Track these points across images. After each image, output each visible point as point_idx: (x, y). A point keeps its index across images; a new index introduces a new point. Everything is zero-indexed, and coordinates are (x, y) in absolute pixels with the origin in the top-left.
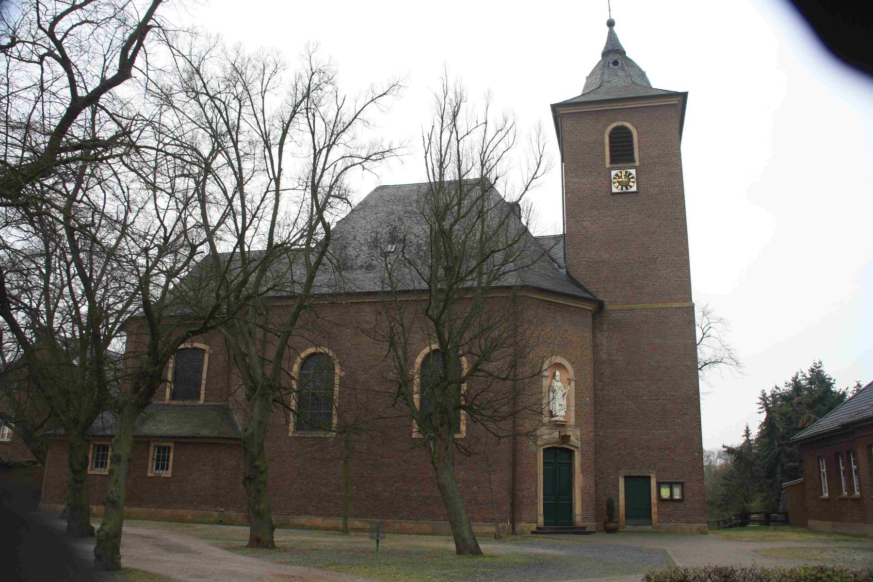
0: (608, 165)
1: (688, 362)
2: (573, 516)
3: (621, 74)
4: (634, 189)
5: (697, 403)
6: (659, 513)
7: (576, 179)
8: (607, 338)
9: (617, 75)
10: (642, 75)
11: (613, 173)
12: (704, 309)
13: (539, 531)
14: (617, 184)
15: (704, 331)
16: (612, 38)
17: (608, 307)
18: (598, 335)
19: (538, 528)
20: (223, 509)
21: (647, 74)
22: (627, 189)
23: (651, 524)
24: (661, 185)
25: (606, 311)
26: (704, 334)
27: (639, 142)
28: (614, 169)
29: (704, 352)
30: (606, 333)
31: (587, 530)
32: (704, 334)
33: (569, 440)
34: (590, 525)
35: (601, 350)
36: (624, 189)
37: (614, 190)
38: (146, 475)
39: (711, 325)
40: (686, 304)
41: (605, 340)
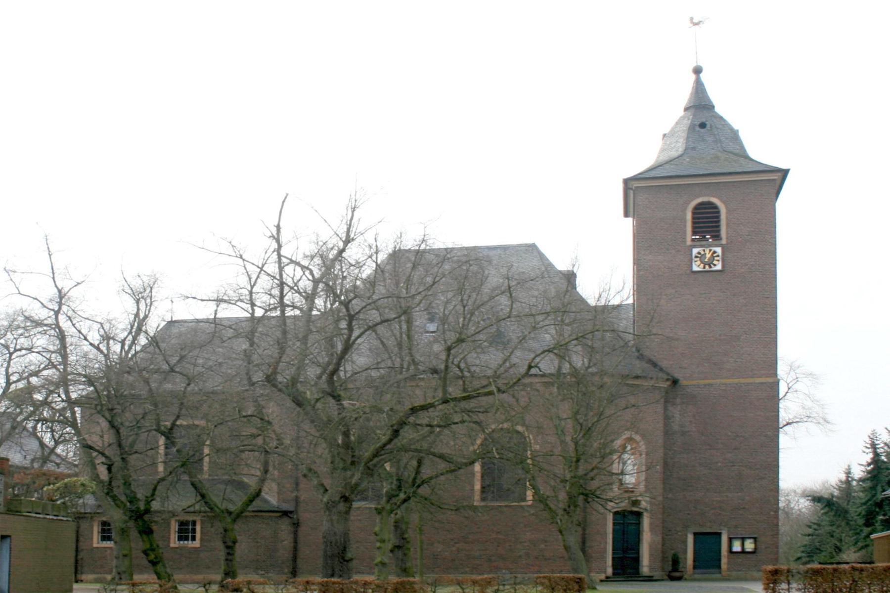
0: (689, 236)
1: (769, 433)
2: (640, 567)
3: (710, 139)
4: (719, 267)
5: (773, 229)
6: (729, 563)
7: (650, 256)
8: (680, 411)
9: (704, 140)
10: (734, 136)
11: (695, 251)
12: (792, 363)
13: (607, 579)
14: (699, 263)
15: (790, 385)
16: (699, 89)
17: (683, 382)
18: (670, 408)
19: (607, 577)
20: (263, 572)
21: (742, 135)
22: (710, 267)
23: (720, 573)
24: (751, 263)
25: (680, 386)
26: (789, 389)
27: (727, 218)
28: (695, 247)
29: (787, 409)
30: (679, 407)
31: (654, 578)
32: (789, 389)
33: (639, 504)
34: (657, 574)
35: (673, 422)
36: (707, 267)
37: (695, 268)
38: (169, 546)
39: (799, 379)
40: (770, 380)
41: (678, 413)
